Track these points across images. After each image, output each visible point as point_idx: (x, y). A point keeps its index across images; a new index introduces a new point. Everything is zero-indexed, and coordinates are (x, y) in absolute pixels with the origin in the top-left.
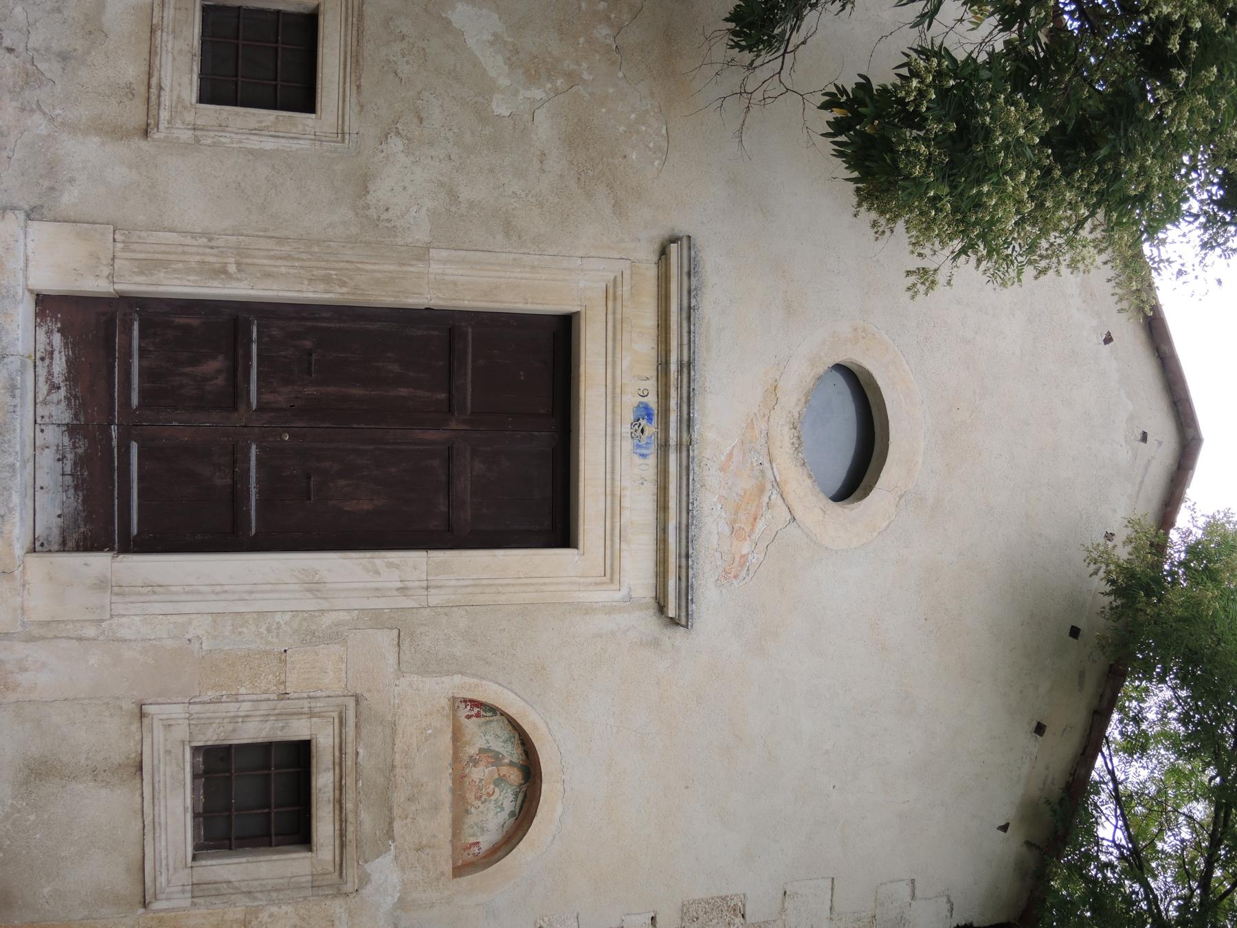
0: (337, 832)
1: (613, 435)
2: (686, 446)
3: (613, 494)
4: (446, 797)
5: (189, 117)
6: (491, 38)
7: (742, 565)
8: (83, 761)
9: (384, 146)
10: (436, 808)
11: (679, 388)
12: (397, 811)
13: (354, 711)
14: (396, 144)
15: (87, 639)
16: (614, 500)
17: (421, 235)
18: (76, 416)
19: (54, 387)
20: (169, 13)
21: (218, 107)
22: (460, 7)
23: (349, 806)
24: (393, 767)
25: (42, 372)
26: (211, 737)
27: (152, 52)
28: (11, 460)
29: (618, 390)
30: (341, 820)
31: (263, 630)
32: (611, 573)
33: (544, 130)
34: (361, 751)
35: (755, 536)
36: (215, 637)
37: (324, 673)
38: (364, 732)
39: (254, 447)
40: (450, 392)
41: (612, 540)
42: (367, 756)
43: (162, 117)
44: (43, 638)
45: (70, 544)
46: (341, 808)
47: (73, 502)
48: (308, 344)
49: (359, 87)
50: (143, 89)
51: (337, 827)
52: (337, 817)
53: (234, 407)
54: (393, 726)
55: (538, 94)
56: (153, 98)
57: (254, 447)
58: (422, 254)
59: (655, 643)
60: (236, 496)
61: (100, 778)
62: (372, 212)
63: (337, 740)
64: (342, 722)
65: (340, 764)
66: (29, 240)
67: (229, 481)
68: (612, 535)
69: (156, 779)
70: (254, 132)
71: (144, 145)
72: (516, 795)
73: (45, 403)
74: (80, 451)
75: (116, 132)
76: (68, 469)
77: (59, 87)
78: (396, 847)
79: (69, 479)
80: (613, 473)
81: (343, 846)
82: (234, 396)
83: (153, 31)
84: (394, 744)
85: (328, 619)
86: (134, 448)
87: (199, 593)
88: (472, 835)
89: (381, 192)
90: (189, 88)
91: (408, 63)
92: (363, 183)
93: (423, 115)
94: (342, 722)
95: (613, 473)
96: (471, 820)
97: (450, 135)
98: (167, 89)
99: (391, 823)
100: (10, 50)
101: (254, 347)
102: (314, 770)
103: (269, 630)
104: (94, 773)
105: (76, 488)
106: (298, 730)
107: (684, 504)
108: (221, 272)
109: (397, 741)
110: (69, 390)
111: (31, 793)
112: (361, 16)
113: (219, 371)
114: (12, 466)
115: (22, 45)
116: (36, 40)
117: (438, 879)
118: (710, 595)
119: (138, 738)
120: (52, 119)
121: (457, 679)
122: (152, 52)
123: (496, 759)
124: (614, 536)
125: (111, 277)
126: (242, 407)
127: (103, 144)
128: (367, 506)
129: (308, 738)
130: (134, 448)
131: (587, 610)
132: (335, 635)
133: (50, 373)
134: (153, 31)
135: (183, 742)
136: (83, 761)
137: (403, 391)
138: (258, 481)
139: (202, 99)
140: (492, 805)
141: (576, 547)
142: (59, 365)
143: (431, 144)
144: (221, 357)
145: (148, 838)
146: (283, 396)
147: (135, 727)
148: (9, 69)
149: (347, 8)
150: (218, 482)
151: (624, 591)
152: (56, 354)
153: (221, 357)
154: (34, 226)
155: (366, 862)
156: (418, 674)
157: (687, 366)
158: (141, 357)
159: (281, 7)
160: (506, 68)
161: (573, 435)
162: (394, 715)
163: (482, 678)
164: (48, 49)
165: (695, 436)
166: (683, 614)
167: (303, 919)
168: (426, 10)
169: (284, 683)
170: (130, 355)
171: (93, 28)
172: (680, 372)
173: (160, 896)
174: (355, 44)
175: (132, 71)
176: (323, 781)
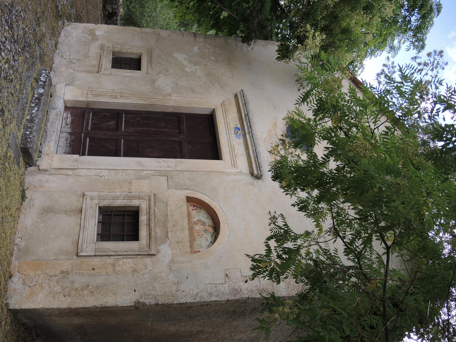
0: (148, 234)
1: (229, 133)
2: (251, 132)
3: (231, 146)
4: (186, 226)
8: (62, 208)
10: (183, 229)
11: (246, 120)
12: (169, 230)
13: (153, 199)
14: (161, 75)
15: (69, 175)
16: (232, 149)
17: (170, 91)
20: (105, 54)
22: (176, 54)
23: (152, 225)
24: (167, 215)
25: (64, 121)
26: (105, 203)
29: (228, 123)
30: (149, 230)
31: (124, 174)
32: (234, 165)
33: (199, 73)
34: (156, 210)
36: (109, 176)
37: (145, 187)
38: (157, 205)
40: (180, 130)
41: (233, 157)
42: (158, 211)
44: (55, 174)
46: (149, 226)
48: (138, 119)
50: (98, 66)
51: (148, 232)
52: (148, 229)
55: (197, 68)
57: (123, 140)
58: (170, 95)
59: (252, 184)
61: (67, 213)
62: (156, 87)
63: (148, 206)
64: (150, 200)
65: (149, 213)
67: (115, 148)
68: (233, 156)
69: (86, 213)
71: (97, 74)
72: (212, 236)
73: (64, 128)
75: (90, 72)
76: (68, 142)
78: (169, 242)
79: (68, 145)
80: (230, 141)
82: (118, 128)
83: (101, 56)
84: (167, 208)
86: (88, 139)
88: (198, 248)
89: (158, 83)
90: (109, 65)
92: (153, 82)
94: (150, 200)
95: (230, 141)
96: (197, 242)
99: (167, 233)
101: (124, 119)
102: (140, 215)
103: (126, 175)
104: (66, 212)
105: (70, 147)
106: (135, 203)
107: (253, 145)
108: (116, 97)
109: (168, 208)
111: (43, 217)
112: (151, 55)
113: (113, 124)
114: (54, 131)
117: (185, 254)
119: (82, 202)
121: (187, 191)
123: (204, 224)
124: (233, 157)
125: (86, 97)
129: (138, 205)
130: (88, 139)
131: (228, 174)
132: (146, 177)
133: (66, 122)
135: (96, 204)
136: (62, 208)
137: (166, 130)
139: (113, 67)
140: (204, 239)
141: (222, 160)
142: (69, 120)
143: (171, 75)
144: (114, 121)
145: (81, 231)
146: (131, 130)
147: (81, 199)
150: (112, 148)
152: (69, 118)
153: (114, 121)
154: (67, 87)
155: (159, 245)
156: (174, 189)
157: (247, 115)
161: (217, 139)
162: (167, 200)
163: (196, 191)
165: (253, 129)
166: (259, 172)
167: (135, 265)
169: (131, 189)
170: (89, 119)
171: (86, 56)
172: (246, 117)
173: (83, 251)
175: (95, 63)
176: (143, 218)
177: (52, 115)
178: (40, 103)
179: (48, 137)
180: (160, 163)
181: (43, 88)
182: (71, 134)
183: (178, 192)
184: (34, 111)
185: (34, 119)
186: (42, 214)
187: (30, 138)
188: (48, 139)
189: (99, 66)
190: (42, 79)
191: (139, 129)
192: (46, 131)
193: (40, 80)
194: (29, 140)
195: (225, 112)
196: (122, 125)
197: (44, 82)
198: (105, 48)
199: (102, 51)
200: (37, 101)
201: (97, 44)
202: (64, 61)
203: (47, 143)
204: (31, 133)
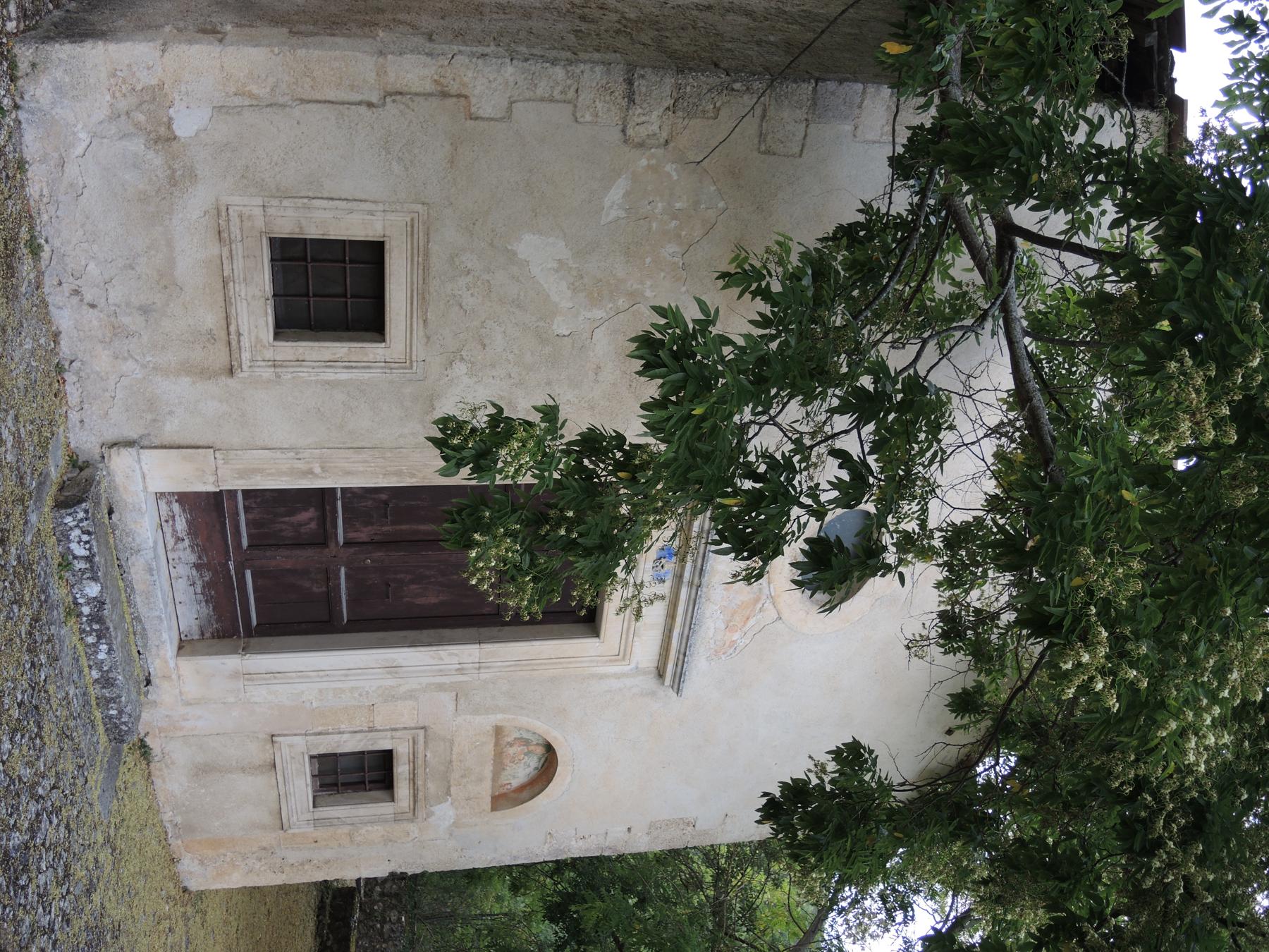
5: (269, 354)
6: (555, 265)
7: (730, 647)
9: (449, 371)
10: (480, 780)
12: (452, 782)
14: (460, 369)
18: (200, 558)
20: (239, 264)
23: (420, 783)
28: (157, 613)
32: (623, 654)
35: (745, 629)
39: (343, 570)
43: (244, 358)
45: (207, 635)
47: (206, 611)
49: (425, 321)
50: (223, 334)
53: (324, 544)
54: (452, 743)
55: (598, 313)
56: (234, 343)
60: (330, 599)
66: (143, 464)
70: (331, 363)
71: (230, 382)
73: (173, 550)
74: (206, 579)
75: (204, 373)
76: (199, 590)
77: (145, 339)
79: (200, 597)
81: (415, 802)
83: (225, 283)
85: (402, 689)
86: (248, 573)
87: (308, 677)
91: (472, 295)
93: (486, 341)
97: (511, 357)
98: (246, 334)
100: (93, 306)
101: (339, 503)
102: (395, 764)
103: (360, 695)
104: (243, 770)
105: (207, 601)
106: (384, 745)
108: (309, 473)
110: (191, 540)
112: (427, 255)
113: (311, 519)
114: (159, 618)
115: (103, 300)
118: (701, 667)
120: (144, 366)
126: (332, 545)
127: (194, 383)
128: (433, 600)
130: (248, 573)
131: (602, 677)
133: (174, 531)
138: (347, 588)
139: (277, 336)
142: (181, 525)
143: (493, 366)
144: (312, 510)
147: (269, 746)
148: (95, 323)
149: (412, 248)
150: (315, 589)
151: (633, 665)
152: (177, 517)
153: (312, 510)
158: (246, 512)
159: (366, 873)
160: (569, 293)
164: (128, 304)
165: (704, 581)
168: (491, 244)
170: (237, 514)
171: (167, 281)
174: (421, 282)
175: (210, 319)
177: (137, 571)
178: (108, 629)
179: (150, 634)
180: (441, 659)
181: (94, 579)
182: (197, 566)
184: (102, 656)
185: (111, 675)
186: (197, 775)
187: (124, 723)
188: (153, 641)
189: (230, 335)
190: (80, 551)
191: (385, 529)
192: (138, 619)
193: (75, 557)
194: (124, 728)
196: (335, 527)
197: (89, 559)
198: (235, 231)
200: (96, 627)
201: (195, 205)
203: (154, 650)
204: (121, 712)
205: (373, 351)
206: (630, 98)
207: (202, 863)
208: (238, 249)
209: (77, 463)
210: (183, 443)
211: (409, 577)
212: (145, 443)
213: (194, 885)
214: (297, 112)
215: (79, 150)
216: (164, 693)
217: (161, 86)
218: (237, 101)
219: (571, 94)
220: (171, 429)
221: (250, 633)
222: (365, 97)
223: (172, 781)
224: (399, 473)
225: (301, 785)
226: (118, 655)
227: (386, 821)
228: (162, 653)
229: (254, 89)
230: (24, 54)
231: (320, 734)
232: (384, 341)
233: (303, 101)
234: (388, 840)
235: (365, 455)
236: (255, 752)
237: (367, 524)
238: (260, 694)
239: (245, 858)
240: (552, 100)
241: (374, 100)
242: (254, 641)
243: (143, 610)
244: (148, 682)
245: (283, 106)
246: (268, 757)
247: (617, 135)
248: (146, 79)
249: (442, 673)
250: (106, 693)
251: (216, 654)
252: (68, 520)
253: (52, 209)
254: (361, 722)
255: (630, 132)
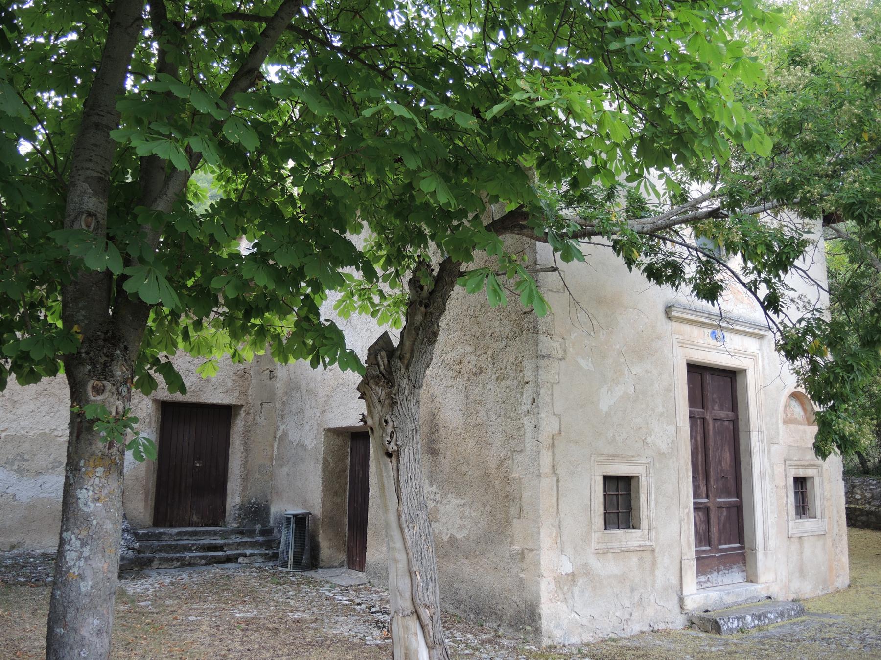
5: (646, 532)
10: (805, 432)
14: (649, 439)
17: (672, 429)
19: (708, 580)
20: (615, 545)
21: (370, 532)
23: (807, 463)
26: (599, 521)
27: (628, 551)
32: (753, 357)
33: (637, 369)
47: (735, 569)
50: (639, 553)
54: (790, 446)
55: (626, 372)
60: (729, 506)
62: (670, 451)
70: (648, 502)
71: (657, 551)
75: (654, 563)
81: (814, 466)
83: (622, 552)
86: (720, 547)
106: (791, 481)
112: (608, 455)
116: (627, 604)
122: (628, 551)
126: (709, 505)
128: (728, 454)
130: (720, 547)
133: (705, 582)
134: (622, 552)
143: (647, 424)
150: (725, 514)
171: (622, 579)
175: (634, 559)
177: (729, 600)
179: (752, 595)
181: (745, 618)
183: (781, 432)
192: (746, 601)
195: (693, 345)
197: (738, 619)
198: (603, 546)
199: (611, 551)
201: (596, 564)
202: (636, 614)
204: (793, 609)
205: (643, 480)
206: (548, 356)
207: (838, 577)
208: (610, 545)
209: (691, 624)
210: (679, 575)
211: (719, 467)
212: (679, 593)
213: (847, 582)
214: (562, 515)
215: (578, 617)
216: (776, 590)
217: (555, 578)
218: (559, 543)
219: (549, 385)
220: (674, 581)
221: (743, 548)
222: (555, 483)
223: (807, 589)
224: (687, 470)
225: (807, 524)
226: (772, 609)
227: (822, 481)
228: (759, 589)
229: (554, 535)
230: (546, 642)
231: (788, 514)
232: (638, 477)
233: (558, 512)
234: (830, 481)
235: (682, 488)
236: (794, 546)
237: (699, 487)
238: (773, 543)
239: (836, 555)
240: (552, 395)
241: (555, 479)
242: (747, 545)
243: (743, 598)
244: (770, 598)
245: (560, 522)
246: (796, 540)
247: (562, 363)
248: (552, 586)
249: (763, 451)
250: (786, 615)
251: (756, 564)
252: (725, 628)
253: (598, 632)
254: (782, 493)
255: (560, 357)
